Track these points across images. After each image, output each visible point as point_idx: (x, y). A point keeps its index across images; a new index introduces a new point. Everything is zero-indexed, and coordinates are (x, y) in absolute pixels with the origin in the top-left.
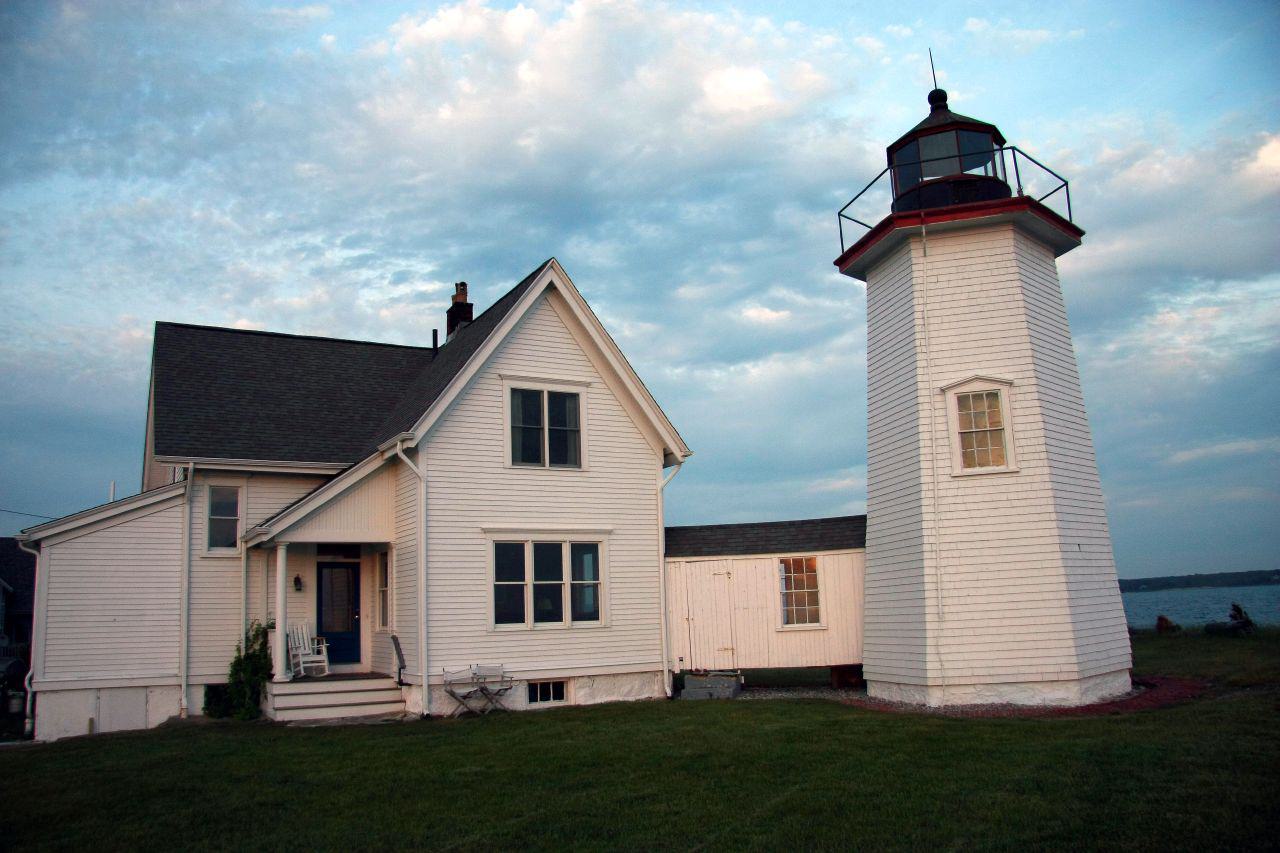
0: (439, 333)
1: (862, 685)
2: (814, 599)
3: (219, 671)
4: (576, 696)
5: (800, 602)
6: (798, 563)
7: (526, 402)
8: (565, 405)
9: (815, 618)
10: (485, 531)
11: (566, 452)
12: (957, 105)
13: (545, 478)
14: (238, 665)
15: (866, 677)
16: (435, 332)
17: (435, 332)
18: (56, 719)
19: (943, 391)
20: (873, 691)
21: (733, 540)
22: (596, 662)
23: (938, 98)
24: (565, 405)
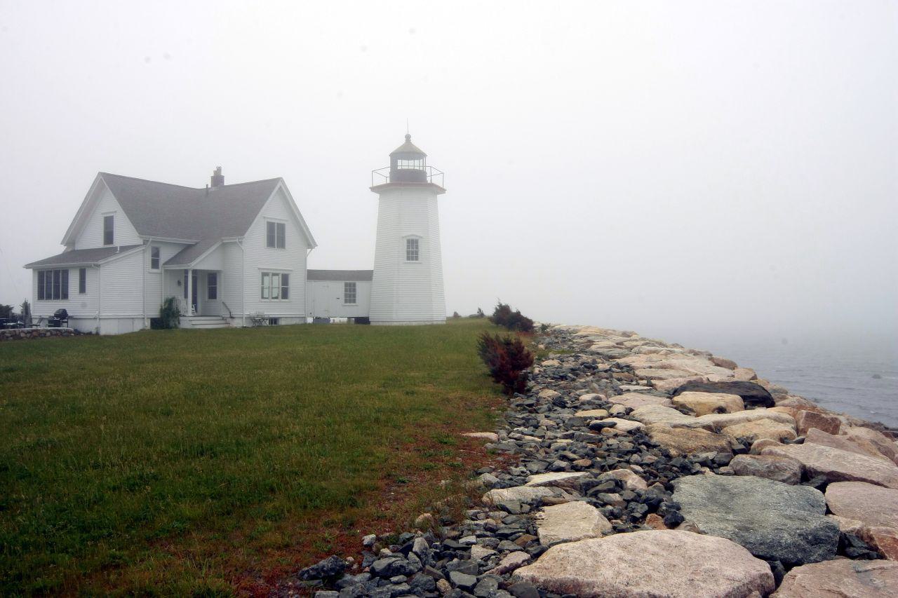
0: (78, 290)
1: (369, 322)
2: (354, 296)
3: (155, 314)
4: (282, 322)
5: (350, 296)
6: (350, 284)
7: (271, 226)
8: (282, 227)
9: (354, 301)
10: (259, 269)
11: (282, 245)
12: (414, 141)
13: (275, 253)
14: (162, 311)
15: (370, 320)
16: (82, 289)
17: (82, 289)
18: (225, 184)
19: (403, 237)
20: (372, 324)
21: (884, 466)
22: (286, 312)
23: (408, 137)
24: (282, 227)
